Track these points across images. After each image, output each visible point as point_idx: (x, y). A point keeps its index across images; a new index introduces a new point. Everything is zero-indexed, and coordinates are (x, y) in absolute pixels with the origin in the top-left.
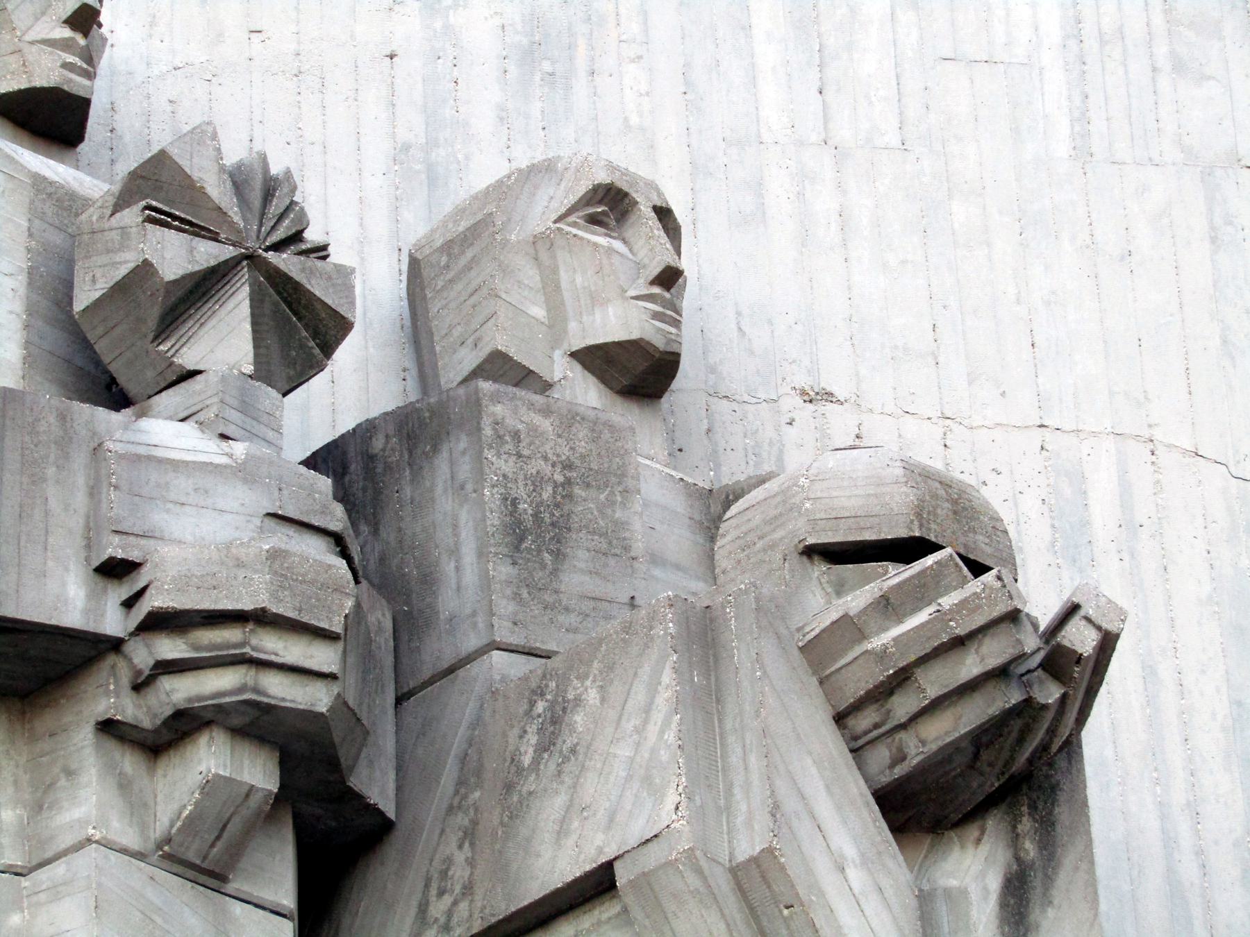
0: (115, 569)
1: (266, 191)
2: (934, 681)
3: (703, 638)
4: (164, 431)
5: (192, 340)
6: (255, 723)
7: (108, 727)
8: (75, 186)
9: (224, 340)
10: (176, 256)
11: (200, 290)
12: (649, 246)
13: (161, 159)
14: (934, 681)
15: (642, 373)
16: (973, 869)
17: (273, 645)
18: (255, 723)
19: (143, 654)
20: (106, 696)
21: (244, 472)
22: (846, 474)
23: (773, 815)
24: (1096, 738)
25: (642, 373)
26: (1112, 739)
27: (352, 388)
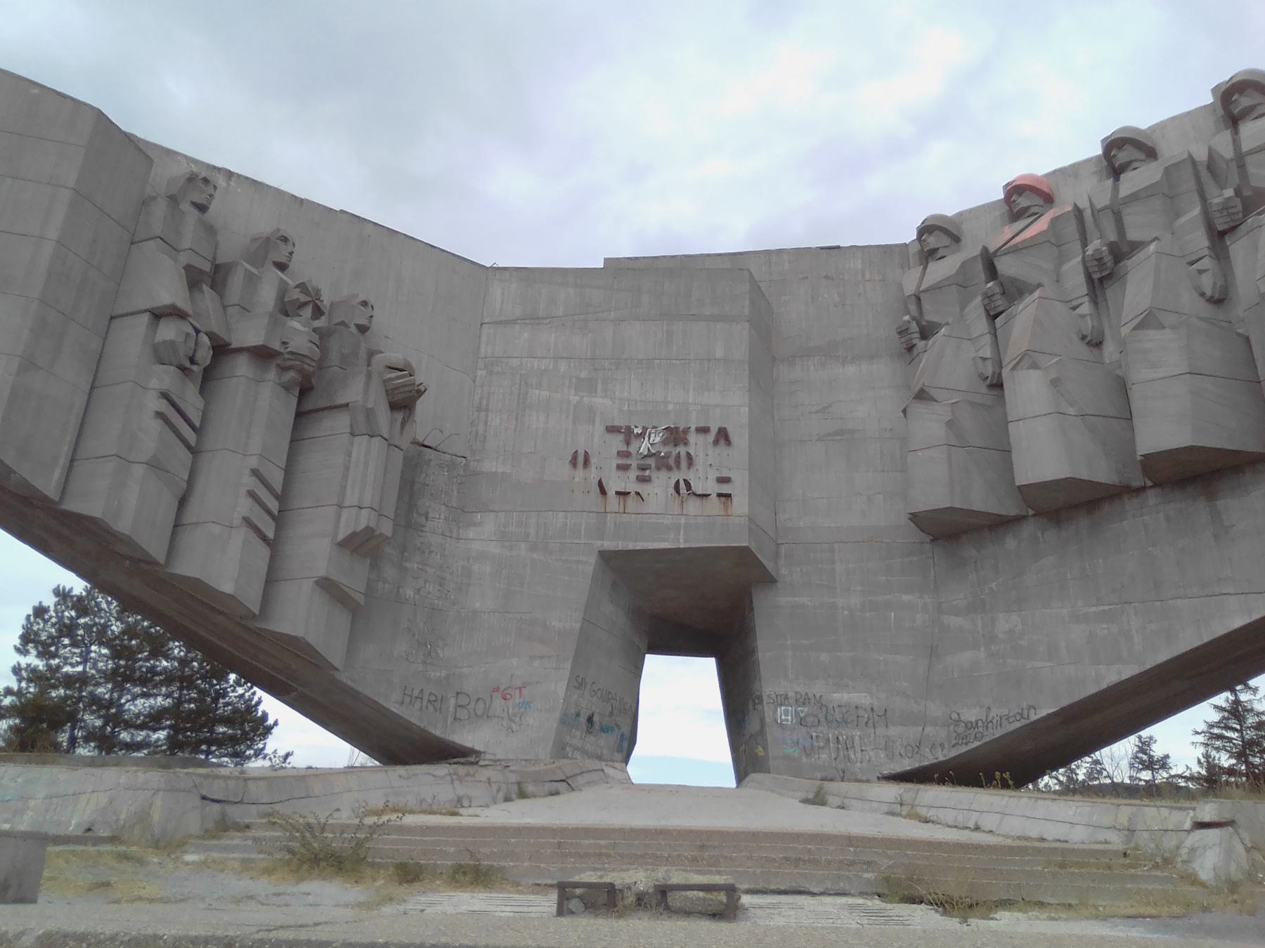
0: (284, 343)
1: (318, 291)
3: (369, 375)
6: (300, 371)
8: (1052, 832)
10: (303, 298)
11: (303, 305)
13: (303, 283)
14: (401, 390)
15: (363, 329)
16: (399, 416)
18: (300, 371)
22: (396, 357)
23: (971, 906)
25: (363, 329)
26: (421, 405)
27: (321, 323)
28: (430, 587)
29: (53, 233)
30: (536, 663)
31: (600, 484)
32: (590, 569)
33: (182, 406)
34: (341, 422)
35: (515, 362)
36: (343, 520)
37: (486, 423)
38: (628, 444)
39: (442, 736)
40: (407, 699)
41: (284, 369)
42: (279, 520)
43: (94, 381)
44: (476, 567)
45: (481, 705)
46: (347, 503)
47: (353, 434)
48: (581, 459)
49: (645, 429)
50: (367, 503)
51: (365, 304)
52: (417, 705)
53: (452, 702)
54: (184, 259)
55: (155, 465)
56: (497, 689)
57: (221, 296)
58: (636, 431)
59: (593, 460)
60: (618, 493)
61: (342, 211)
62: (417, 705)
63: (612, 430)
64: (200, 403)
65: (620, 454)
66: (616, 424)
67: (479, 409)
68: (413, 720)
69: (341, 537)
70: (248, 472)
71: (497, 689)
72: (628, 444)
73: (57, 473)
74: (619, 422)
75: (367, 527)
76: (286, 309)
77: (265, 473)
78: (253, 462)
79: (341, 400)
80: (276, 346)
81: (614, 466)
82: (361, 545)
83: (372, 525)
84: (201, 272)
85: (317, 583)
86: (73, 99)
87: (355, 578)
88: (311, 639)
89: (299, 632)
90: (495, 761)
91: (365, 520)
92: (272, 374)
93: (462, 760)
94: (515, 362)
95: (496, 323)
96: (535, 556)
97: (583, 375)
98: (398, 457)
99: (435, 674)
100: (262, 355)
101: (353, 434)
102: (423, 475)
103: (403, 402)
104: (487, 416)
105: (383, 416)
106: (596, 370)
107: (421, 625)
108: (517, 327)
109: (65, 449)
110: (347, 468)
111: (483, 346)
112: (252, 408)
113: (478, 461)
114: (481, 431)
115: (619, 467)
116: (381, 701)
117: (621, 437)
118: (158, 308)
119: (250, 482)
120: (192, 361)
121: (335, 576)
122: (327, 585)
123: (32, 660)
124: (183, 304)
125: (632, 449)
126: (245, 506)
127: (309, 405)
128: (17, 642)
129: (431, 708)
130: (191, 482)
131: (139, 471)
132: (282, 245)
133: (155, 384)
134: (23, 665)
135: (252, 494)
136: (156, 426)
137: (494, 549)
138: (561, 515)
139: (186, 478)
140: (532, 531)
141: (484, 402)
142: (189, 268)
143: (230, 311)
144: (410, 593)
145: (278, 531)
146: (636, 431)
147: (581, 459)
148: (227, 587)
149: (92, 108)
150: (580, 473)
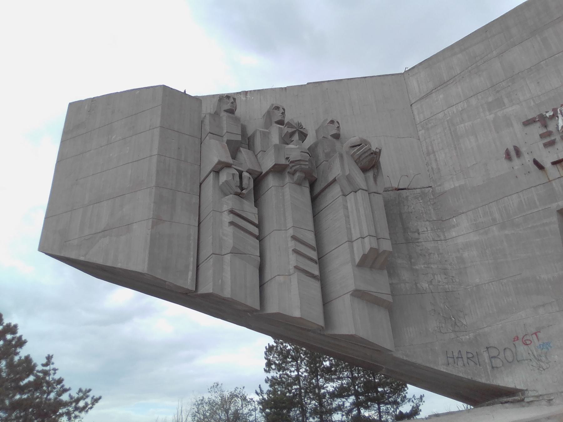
0: (287, 158)
1: (300, 126)
2: (363, 156)
3: (341, 156)
4: (291, 146)
5: (507, 405)
6: (302, 171)
7: (288, 172)
9: (296, 137)
10: (290, 130)
11: (292, 134)
12: (337, 125)
14: (363, 156)
15: (337, 136)
16: (370, 174)
17: (302, 163)
18: (302, 171)
19: (291, 165)
20: (288, 170)
21: (298, 148)
22: (354, 140)
24: (381, 160)
26: (384, 160)
27: (309, 141)
28: (438, 278)
29: (155, 152)
30: (541, 311)
31: (536, 162)
32: (556, 227)
33: (244, 215)
34: (336, 191)
35: (441, 115)
36: (355, 249)
37: (436, 160)
38: (546, 126)
39: (488, 382)
40: (451, 360)
41: (293, 174)
42: (321, 261)
43: (199, 219)
44: (466, 255)
45: (508, 353)
46: (354, 239)
47: (345, 195)
48: (513, 153)
49: (555, 110)
50: (366, 233)
51: (332, 122)
52: (460, 363)
53: (486, 355)
54: (225, 139)
55: (235, 252)
56: (517, 338)
57: (254, 152)
58: (548, 115)
59: (523, 149)
60: (554, 163)
61: (308, 84)
62: (460, 363)
63: (528, 123)
64: (255, 210)
65: (542, 136)
66: (530, 117)
67: (428, 154)
68: (461, 375)
69: (357, 260)
70: (290, 239)
71: (517, 338)
72: (546, 126)
73: (191, 274)
74: (531, 115)
75: (371, 248)
76: (286, 139)
77: (300, 236)
78: (291, 232)
79: (331, 179)
80: (283, 161)
81: (541, 146)
82: (371, 261)
83: (375, 246)
84: (237, 141)
85: (352, 295)
86: (152, 87)
87: (379, 284)
88: (362, 334)
89: (352, 332)
90: (538, 397)
91: (368, 244)
92: (287, 179)
93: (510, 399)
94: (441, 115)
95: (419, 100)
96: (506, 232)
97: (490, 99)
98: (379, 200)
99: (465, 338)
100: (278, 170)
101: (345, 195)
102: (406, 207)
103: (370, 163)
104: (435, 155)
105: (359, 178)
106: (498, 92)
107: (442, 305)
108: (434, 95)
109: (192, 260)
110: (347, 217)
111: (417, 117)
112: (285, 201)
113: (440, 185)
114: (434, 166)
115: (546, 145)
116: (432, 366)
117: (538, 125)
118: (215, 167)
119: (292, 244)
120: (242, 189)
121: (363, 287)
122: (358, 294)
123: (274, 374)
124: (230, 161)
125: (552, 127)
126: (293, 260)
127: (318, 189)
128: (264, 366)
129: (472, 363)
130: (262, 256)
131: (228, 258)
132: (276, 111)
133: (226, 208)
134: (270, 378)
135: (295, 251)
136: (229, 230)
137: (473, 237)
138: (514, 196)
139: (258, 254)
140: (497, 216)
141: (430, 148)
142: (229, 142)
143: (259, 156)
144: (425, 285)
145: (322, 269)
146: (548, 115)
147: (513, 153)
148: (297, 314)
149: (160, 86)
150: (516, 162)
